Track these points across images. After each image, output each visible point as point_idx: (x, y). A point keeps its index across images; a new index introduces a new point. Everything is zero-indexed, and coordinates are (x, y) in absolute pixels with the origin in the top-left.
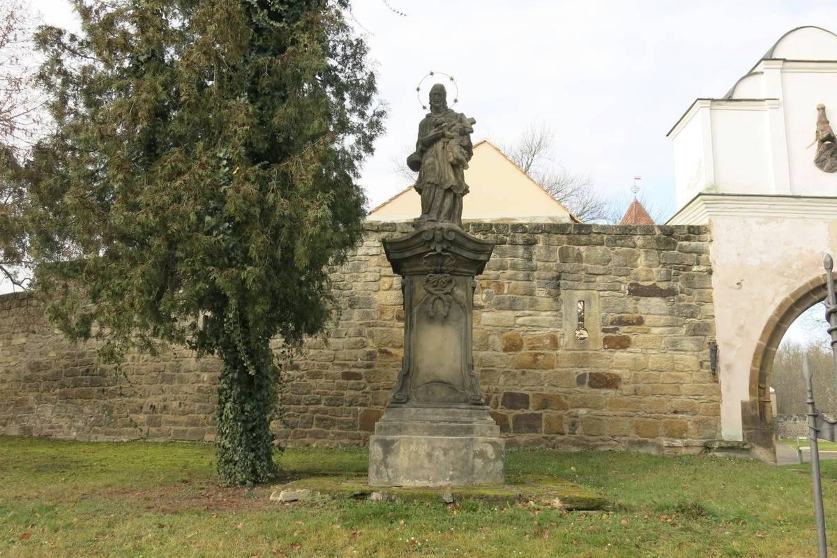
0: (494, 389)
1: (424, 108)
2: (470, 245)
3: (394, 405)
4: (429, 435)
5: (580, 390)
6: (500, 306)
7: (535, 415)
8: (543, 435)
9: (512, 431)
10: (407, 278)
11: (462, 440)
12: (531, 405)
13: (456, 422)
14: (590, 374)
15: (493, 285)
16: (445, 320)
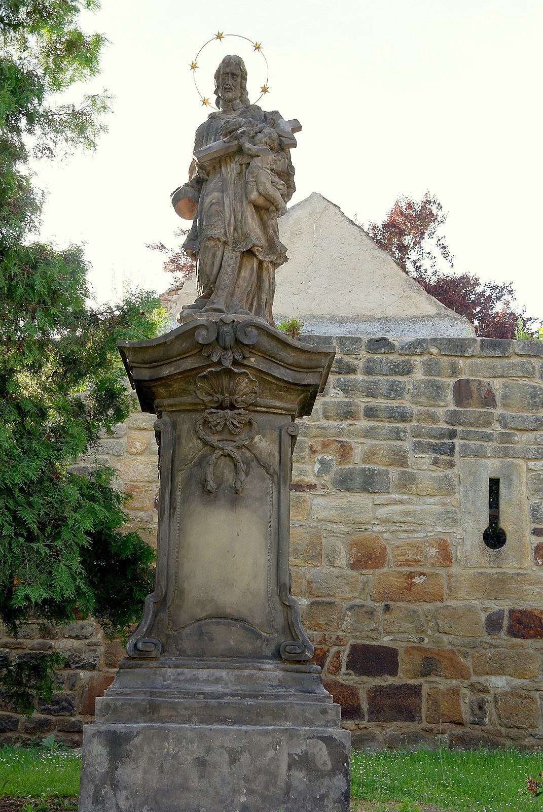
0: (334, 638)
1: (205, 102)
2: (290, 356)
3: (132, 662)
4: (201, 722)
5: (493, 642)
6: (344, 483)
7: (409, 687)
8: (424, 725)
9: (367, 718)
10: (165, 417)
11: (267, 733)
12: (402, 667)
13: (256, 697)
14: (512, 612)
15: (333, 446)
16: (235, 497)
